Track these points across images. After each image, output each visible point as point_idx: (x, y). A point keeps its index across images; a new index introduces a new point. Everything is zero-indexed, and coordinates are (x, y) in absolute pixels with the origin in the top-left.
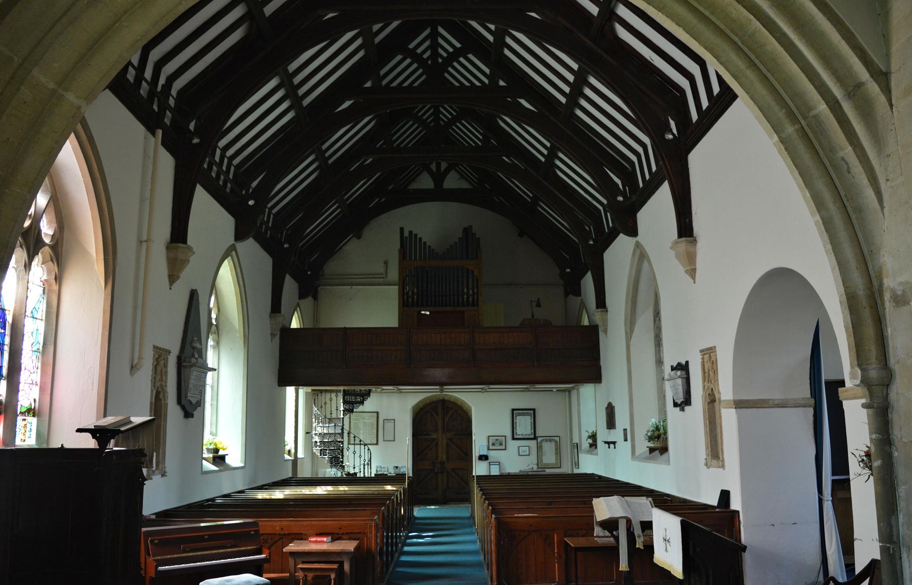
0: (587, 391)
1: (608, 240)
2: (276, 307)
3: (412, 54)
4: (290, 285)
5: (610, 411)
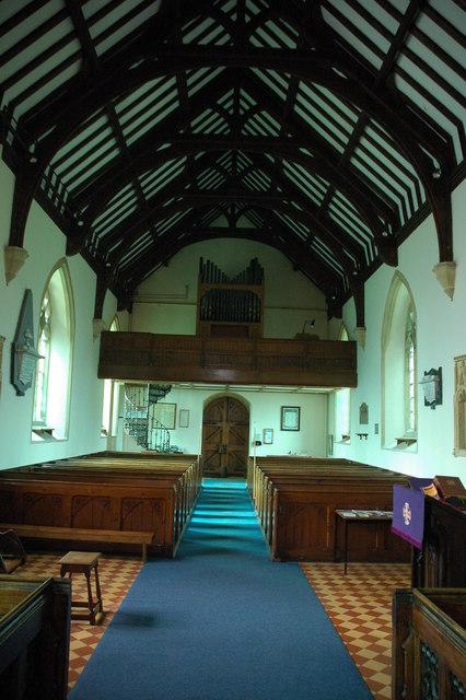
0: (343, 395)
1: (368, 271)
2: (98, 314)
3: (219, 108)
4: (110, 299)
5: (364, 410)
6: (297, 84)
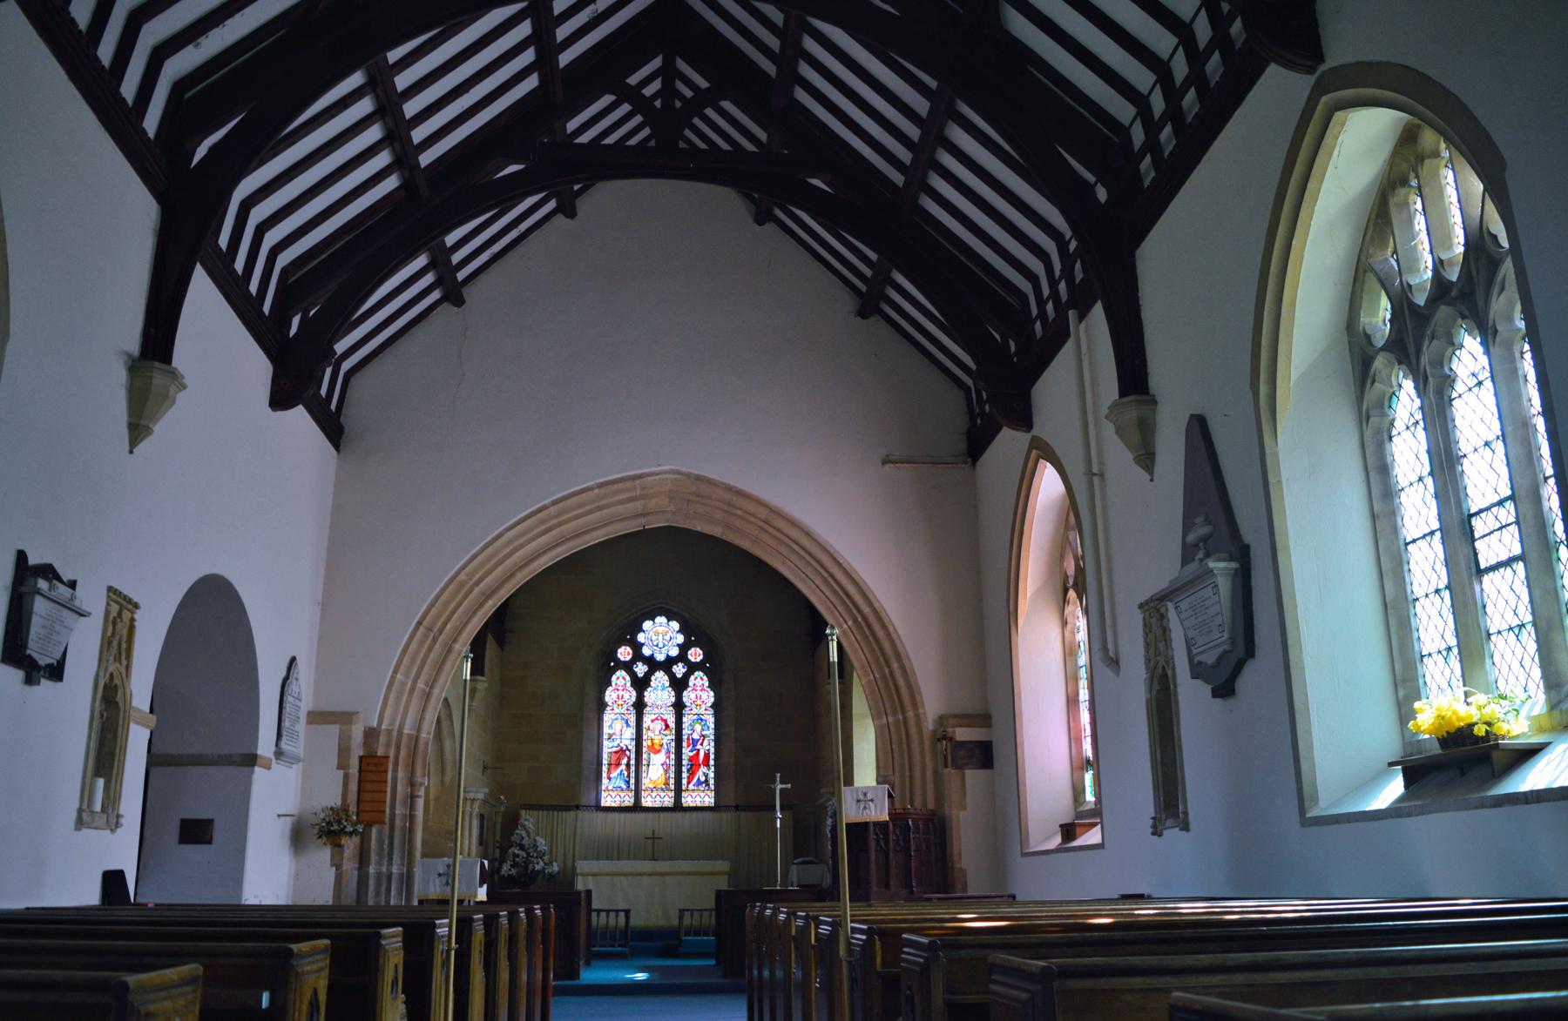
3: (632, 95)
6: (799, 42)
